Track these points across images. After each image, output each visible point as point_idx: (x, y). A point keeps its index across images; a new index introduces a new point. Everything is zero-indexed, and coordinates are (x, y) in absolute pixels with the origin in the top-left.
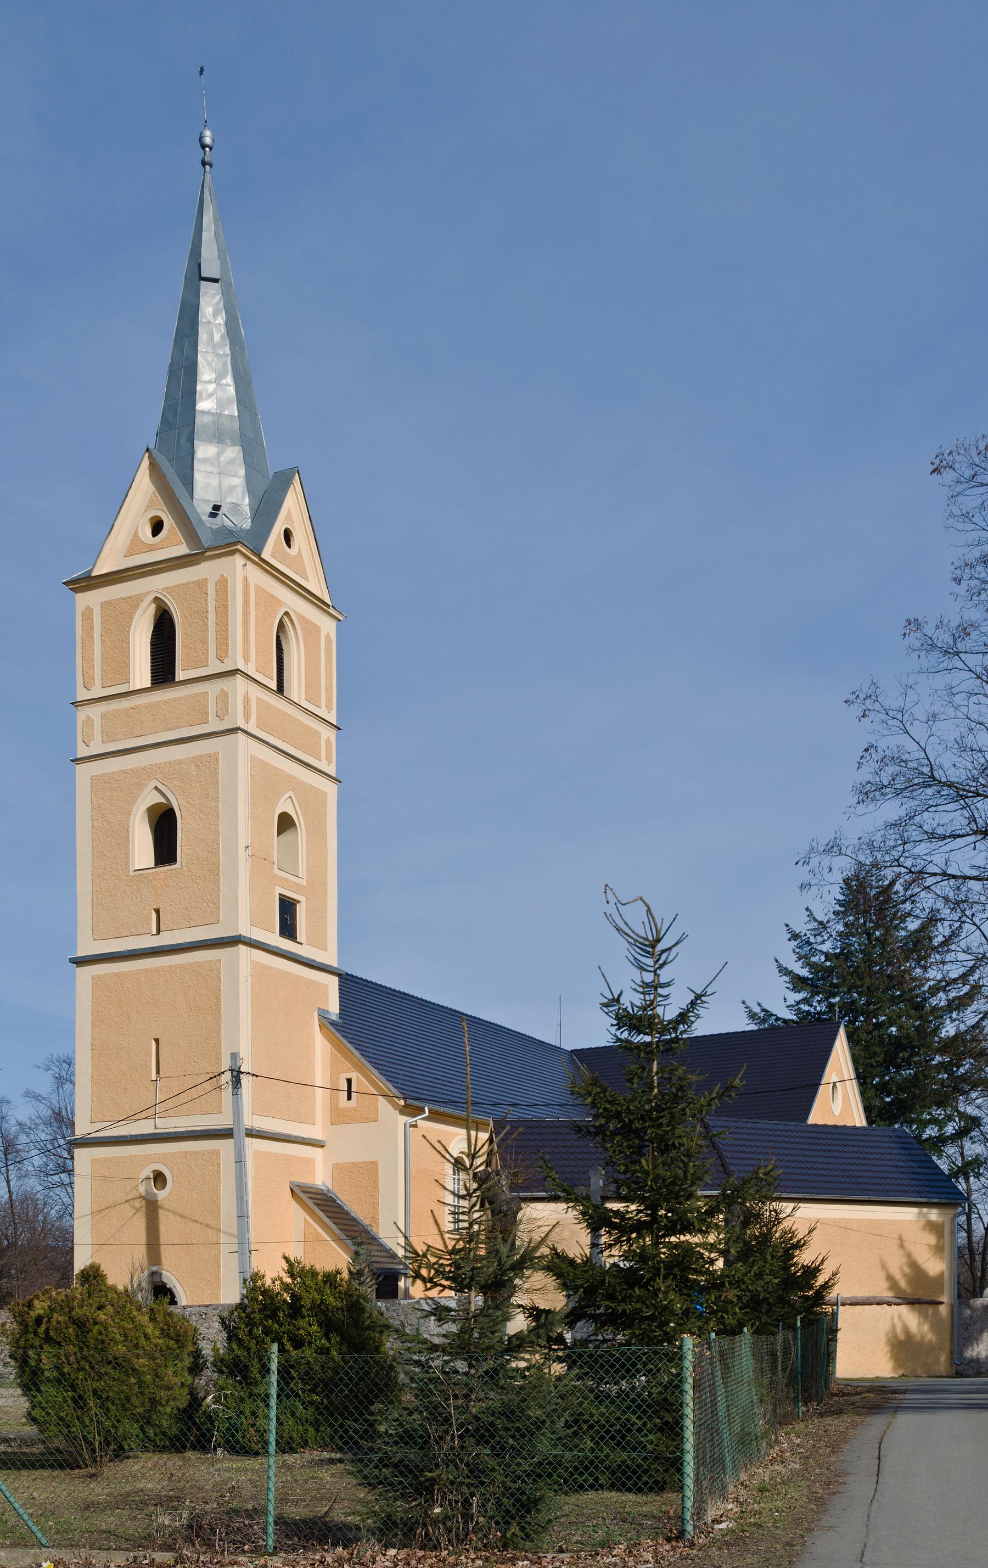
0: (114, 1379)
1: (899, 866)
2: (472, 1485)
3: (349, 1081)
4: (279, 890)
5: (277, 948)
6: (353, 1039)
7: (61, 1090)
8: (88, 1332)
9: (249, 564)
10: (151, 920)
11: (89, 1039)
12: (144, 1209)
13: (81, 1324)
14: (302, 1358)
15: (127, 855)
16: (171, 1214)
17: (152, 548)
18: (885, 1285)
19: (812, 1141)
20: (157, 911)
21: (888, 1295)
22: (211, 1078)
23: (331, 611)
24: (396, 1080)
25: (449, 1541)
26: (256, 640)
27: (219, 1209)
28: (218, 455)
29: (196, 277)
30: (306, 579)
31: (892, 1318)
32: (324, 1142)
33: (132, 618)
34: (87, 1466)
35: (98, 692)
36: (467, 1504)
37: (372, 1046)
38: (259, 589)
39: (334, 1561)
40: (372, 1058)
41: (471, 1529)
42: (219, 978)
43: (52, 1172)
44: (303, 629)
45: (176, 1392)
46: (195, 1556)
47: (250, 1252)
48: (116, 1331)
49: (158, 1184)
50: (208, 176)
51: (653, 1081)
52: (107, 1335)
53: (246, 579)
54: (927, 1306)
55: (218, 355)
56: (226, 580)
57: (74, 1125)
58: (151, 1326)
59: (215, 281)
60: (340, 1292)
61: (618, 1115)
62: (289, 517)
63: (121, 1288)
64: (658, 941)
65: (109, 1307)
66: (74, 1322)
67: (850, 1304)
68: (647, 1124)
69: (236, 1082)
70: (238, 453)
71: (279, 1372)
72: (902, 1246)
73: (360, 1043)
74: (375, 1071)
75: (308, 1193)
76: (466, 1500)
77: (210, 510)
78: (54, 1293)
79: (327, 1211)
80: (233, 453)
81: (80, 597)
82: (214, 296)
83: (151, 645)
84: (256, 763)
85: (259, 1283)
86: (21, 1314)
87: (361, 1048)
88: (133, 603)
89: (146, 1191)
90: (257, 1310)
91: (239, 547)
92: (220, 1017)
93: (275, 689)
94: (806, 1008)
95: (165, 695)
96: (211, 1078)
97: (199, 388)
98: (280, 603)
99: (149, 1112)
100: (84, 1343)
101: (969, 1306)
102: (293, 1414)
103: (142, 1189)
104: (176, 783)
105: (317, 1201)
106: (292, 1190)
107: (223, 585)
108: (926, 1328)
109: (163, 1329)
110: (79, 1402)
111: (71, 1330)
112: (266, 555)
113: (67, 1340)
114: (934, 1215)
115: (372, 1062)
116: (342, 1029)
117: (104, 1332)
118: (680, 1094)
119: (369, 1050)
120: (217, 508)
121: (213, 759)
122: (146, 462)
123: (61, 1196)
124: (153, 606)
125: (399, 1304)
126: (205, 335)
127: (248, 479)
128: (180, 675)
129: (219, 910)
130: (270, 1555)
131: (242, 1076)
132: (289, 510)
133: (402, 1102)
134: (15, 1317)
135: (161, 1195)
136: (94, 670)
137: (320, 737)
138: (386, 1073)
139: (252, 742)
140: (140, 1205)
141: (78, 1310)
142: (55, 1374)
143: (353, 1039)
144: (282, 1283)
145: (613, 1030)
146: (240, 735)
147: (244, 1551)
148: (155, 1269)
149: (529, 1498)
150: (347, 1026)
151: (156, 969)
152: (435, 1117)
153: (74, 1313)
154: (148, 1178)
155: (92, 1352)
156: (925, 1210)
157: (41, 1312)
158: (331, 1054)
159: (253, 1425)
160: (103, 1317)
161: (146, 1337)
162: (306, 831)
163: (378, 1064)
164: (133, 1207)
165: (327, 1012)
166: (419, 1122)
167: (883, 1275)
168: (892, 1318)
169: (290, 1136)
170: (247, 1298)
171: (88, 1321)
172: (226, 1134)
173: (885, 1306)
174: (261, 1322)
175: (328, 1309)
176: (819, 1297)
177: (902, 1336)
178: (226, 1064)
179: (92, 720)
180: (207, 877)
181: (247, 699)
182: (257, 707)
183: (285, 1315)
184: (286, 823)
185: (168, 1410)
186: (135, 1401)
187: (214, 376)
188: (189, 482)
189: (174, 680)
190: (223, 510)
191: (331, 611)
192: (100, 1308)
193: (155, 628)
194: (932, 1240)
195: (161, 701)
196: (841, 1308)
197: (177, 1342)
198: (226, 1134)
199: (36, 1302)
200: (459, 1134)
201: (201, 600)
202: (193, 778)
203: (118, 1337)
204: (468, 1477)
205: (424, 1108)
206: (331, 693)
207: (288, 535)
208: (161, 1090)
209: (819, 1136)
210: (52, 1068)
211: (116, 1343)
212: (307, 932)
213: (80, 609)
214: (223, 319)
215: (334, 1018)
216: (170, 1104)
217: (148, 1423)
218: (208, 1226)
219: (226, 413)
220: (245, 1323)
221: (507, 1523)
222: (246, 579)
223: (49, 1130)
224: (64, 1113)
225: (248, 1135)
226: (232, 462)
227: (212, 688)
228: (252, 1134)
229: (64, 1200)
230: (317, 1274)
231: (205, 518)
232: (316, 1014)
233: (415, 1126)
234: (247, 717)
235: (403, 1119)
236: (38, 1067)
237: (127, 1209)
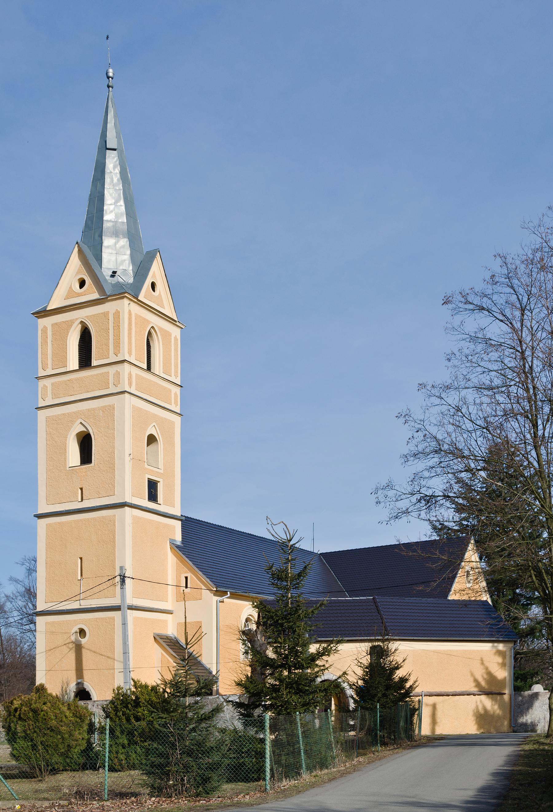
0: (51, 737)
1: (420, 493)
2: (184, 772)
3: (186, 578)
5: (146, 507)
6: (189, 555)
7: (30, 577)
8: (39, 715)
9: (132, 303)
10: (78, 493)
11: (44, 558)
12: (74, 649)
13: (35, 712)
14: (139, 726)
15: (65, 459)
16: (88, 651)
17: (79, 295)
18: (473, 684)
19: (434, 608)
20: (81, 489)
21: (475, 690)
22: (109, 580)
23: (178, 324)
24: (212, 577)
25: (175, 794)
27: (114, 649)
28: (116, 244)
29: (104, 148)
30: (163, 307)
31: (476, 702)
32: (173, 611)
33: (68, 332)
34: (38, 777)
35: (50, 372)
36: (182, 780)
37: (200, 558)
39: (130, 803)
40: (199, 565)
41: (184, 790)
42: (115, 525)
43: (25, 624)
44: (161, 335)
45: (80, 742)
46: (76, 802)
48: (51, 714)
49: (82, 635)
50: (111, 93)
51: (288, 602)
52: (47, 716)
53: (130, 311)
54: (496, 696)
55: (116, 190)
56: (119, 312)
57: (36, 596)
58: (68, 712)
59: (115, 150)
60: (158, 695)
61: (272, 617)
62: (154, 275)
63: (54, 694)
64: (290, 540)
65: (48, 703)
66: (32, 711)
67: (452, 695)
68: (284, 622)
69: (123, 581)
70: (126, 242)
71: (110, 730)
72: (482, 663)
73: (193, 557)
74: (200, 573)
75: (164, 639)
76: (182, 778)
78: (23, 697)
79: (174, 649)
80: (124, 242)
81: (40, 321)
82: (113, 158)
83: (79, 346)
84: (136, 409)
85: (120, 691)
86: (8, 707)
87: (193, 560)
88: (70, 324)
89: (76, 639)
90: (119, 704)
91: (126, 295)
92: (115, 546)
93: (146, 368)
94: (465, 523)
95: (86, 373)
96: (109, 580)
97: (105, 208)
98: (149, 322)
99: (76, 597)
100: (37, 720)
101: (521, 696)
102: (136, 752)
103: (73, 638)
104: (91, 420)
105: (168, 643)
106: (154, 637)
107: (117, 315)
108: (496, 707)
109: (74, 713)
110: (34, 747)
111: (30, 714)
113: (29, 718)
114: (501, 647)
115: (199, 568)
116: (183, 550)
117: (46, 715)
118: (298, 608)
119: (198, 561)
120: (114, 272)
121: (112, 408)
122: (76, 249)
123: (31, 637)
124: (80, 326)
125: (208, 698)
126: (109, 179)
127: (132, 256)
128: (94, 363)
129: (115, 488)
130: (106, 801)
132: (154, 272)
134: (5, 708)
135: (83, 641)
136: (48, 360)
137: (171, 392)
138: (206, 573)
139: (133, 398)
140: (72, 647)
141: (34, 705)
142: (23, 734)
143: (189, 555)
144: (131, 691)
146: (127, 395)
147: (96, 800)
148: (79, 681)
149: (206, 777)
150: (186, 548)
151: (81, 520)
152: (234, 596)
153: (32, 706)
154: (76, 632)
155: (40, 724)
156: (496, 644)
157: (17, 706)
158: (177, 564)
159: (116, 757)
160: (46, 708)
161: (66, 716)
162: (163, 443)
163: (202, 568)
164: (68, 647)
165: (175, 540)
166: (224, 600)
167: (472, 679)
168: (476, 702)
169: (153, 608)
170: (115, 698)
171: (39, 710)
172: (117, 608)
173: (472, 696)
174: (121, 710)
175: (152, 703)
176: (408, 693)
177: (482, 711)
178: (117, 572)
179: (47, 387)
180: (109, 471)
181: (130, 375)
182: (136, 379)
183: (132, 706)
184: (151, 439)
185: (76, 751)
186: (60, 746)
187: (113, 201)
188: (99, 259)
189: (91, 365)
190: (117, 273)
191: (178, 324)
192: (45, 704)
193: (81, 337)
194: (500, 660)
196: (424, 698)
197: (80, 719)
198: (117, 608)
199: (15, 701)
200: (247, 606)
202: (101, 418)
203: (52, 717)
204: (183, 769)
207: (153, 286)
208: (83, 585)
209: (438, 605)
210: (25, 564)
211: (52, 720)
212: (163, 498)
213: (40, 327)
214: (118, 170)
215: (179, 543)
216: (88, 593)
217: (67, 757)
218: (108, 657)
219: (120, 221)
220: (113, 710)
221: (198, 787)
223: (23, 600)
224: (32, 590)
225: (128, 609)
226: (123, 247)
227: (111, 370)
228: (131, 608)
229: (32, 639)
230: (148, 686)
231: (108, 278)
232: (168, 542)
233: (223, 602)
234: (130, 385)
235: (216, 598)
236: (17, 563)
237: (65, 649)
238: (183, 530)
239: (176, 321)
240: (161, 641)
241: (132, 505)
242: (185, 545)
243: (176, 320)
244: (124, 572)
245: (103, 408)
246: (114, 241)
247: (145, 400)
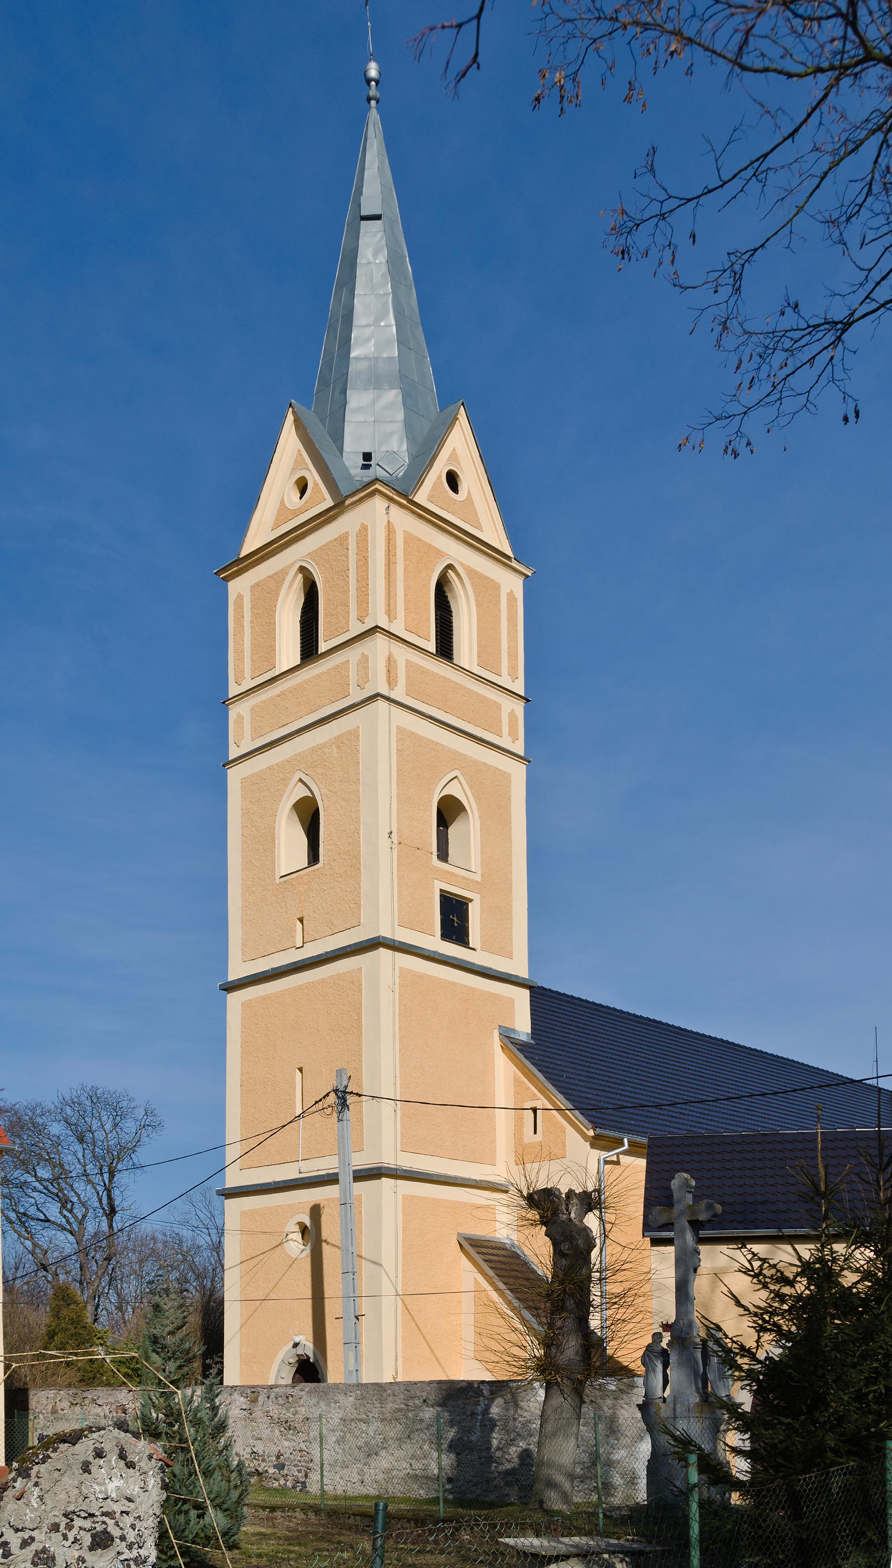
4: (439, 886)
10: (295, 931)
15: (273, 861)
23: (514, 564)
26: (405, 595)
28: (374, 403)
30: (479, 527)
33: (278, 595)
38: (408, 537)
47: (357, 1318)
53: (389, 526)
59: (377, 217)
77: (361, 462)
88: (278, 579)
91: (377, 486)
98: (440, 554)
107: (363, 533)
112: (421, 497)
124: (300, 576)
128: (323, 647)
131: (348, 1097)
133: (591, 1133)
136: (244, 662)
146: (381, 704)
165: (513, 1030)
169: (456, 1178)
181: (390, 661)
188: (338, 437)
191: (514, 564)
195: (305, 681)
201: (342, 558)
205: (622, 1140)
206: (517, 659)
207: (452, 480)
215: (524, 1038)
222: (389, 526)
226: (389, 406)
227: (352, 655)
232: (496, 1033)
233: (617, 1163)
234: (391, 681)
235: (596, 1155)
238: (534, 1013)
239: (509, 558)
241: (396, 944)
242: (539, 1042)
243: (510, 554)
245: (338, 741)
246: (371, 396)
247: (431, 718)
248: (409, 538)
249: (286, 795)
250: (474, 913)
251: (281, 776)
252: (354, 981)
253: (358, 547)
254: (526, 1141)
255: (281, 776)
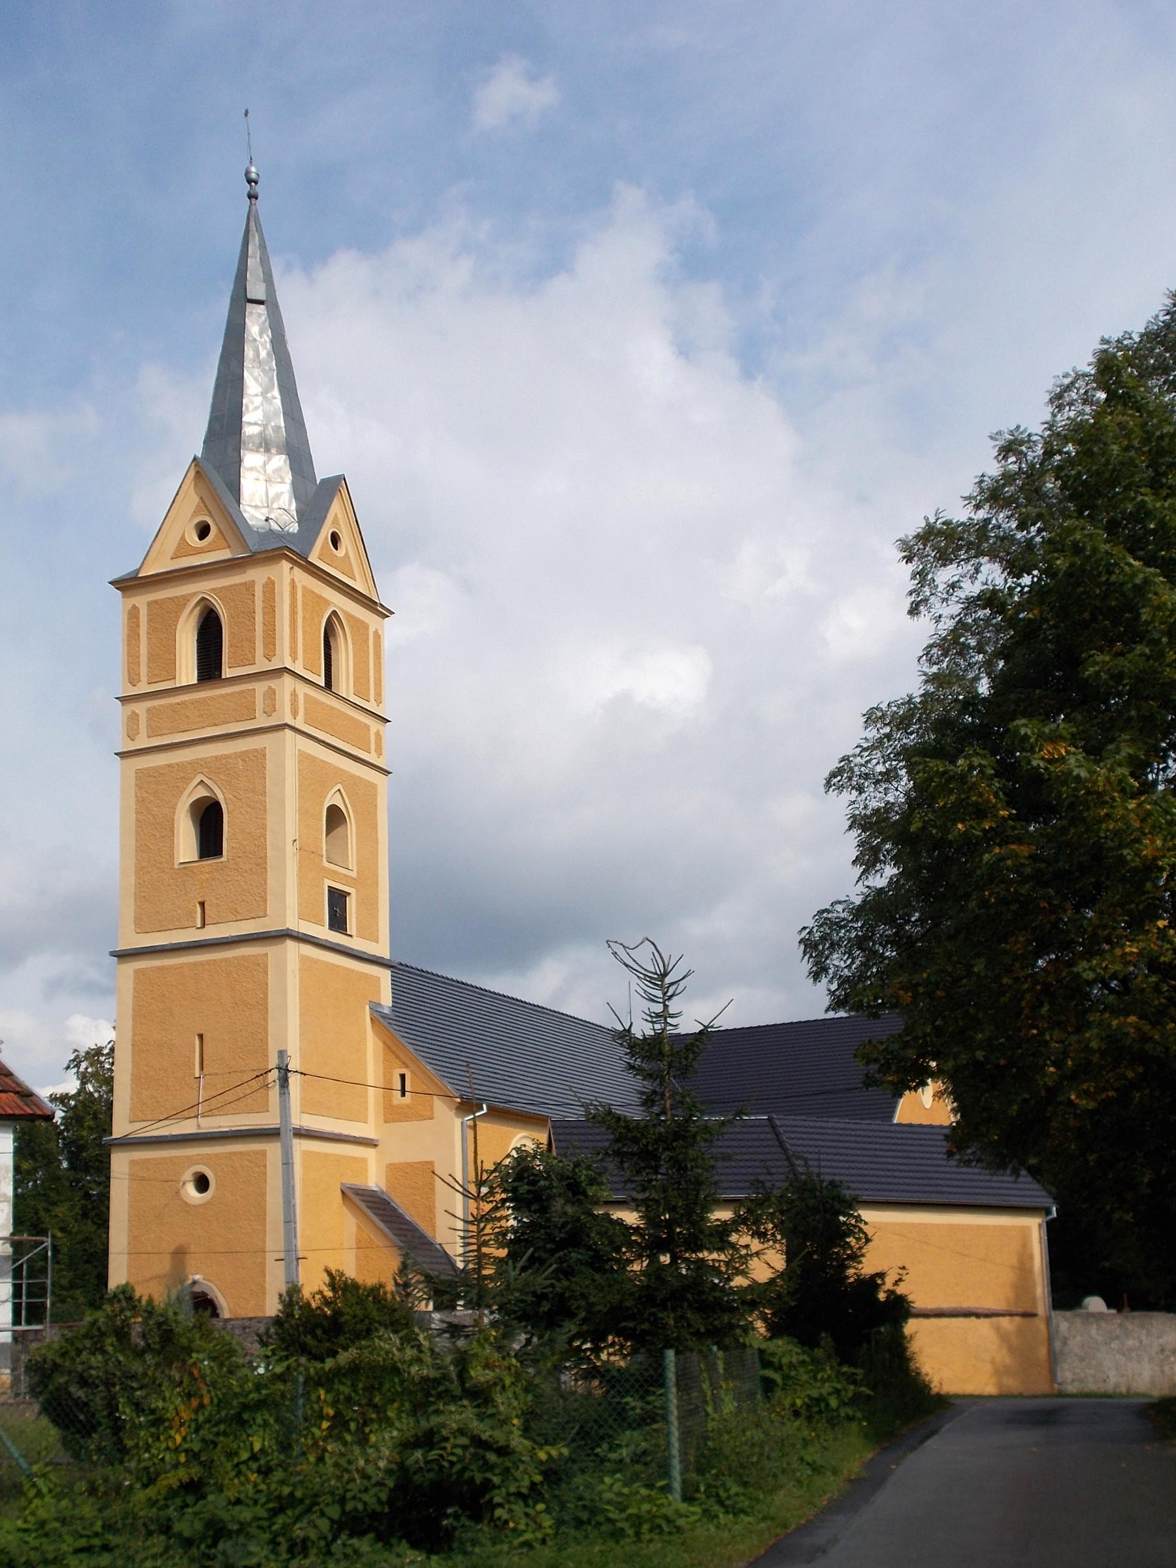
4: (328, 883)
15: (172, 848)
26: (304, 639)
28: (265, 465)
38: (304, 588)
44: (351, 627)
53: (293, 580)
64: (665, 974)
98: (327, 603)
107: (270, 587)
112: (313, 558)
128: (227, 673)
139: (299, 737)
145: (627, 1058)
169: (341, 1135)
172: (271, 1134)
173: (973, 1319)
181: (294, 695)
184: (335, 817)
207: (335, 539)
215: (387, 1011)
226: (278, 471)
227: (260, 687)
232: (367, 1007)
234: (295, 714)
240: (356, 1199)
244: (285, 1063)
245: (244, 755)
247: (324, 742)
248: (307, 591)
249: (186, 793)
250: (352, 905)
251: (182, 774)
252: (261, 966)
253: (264, 596)
254: (395, 1102)
255: (182, 774)
